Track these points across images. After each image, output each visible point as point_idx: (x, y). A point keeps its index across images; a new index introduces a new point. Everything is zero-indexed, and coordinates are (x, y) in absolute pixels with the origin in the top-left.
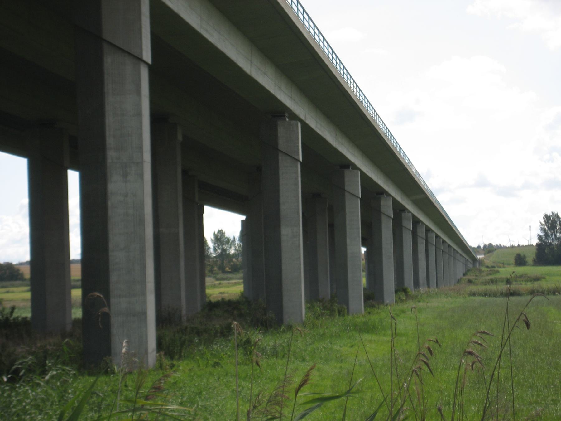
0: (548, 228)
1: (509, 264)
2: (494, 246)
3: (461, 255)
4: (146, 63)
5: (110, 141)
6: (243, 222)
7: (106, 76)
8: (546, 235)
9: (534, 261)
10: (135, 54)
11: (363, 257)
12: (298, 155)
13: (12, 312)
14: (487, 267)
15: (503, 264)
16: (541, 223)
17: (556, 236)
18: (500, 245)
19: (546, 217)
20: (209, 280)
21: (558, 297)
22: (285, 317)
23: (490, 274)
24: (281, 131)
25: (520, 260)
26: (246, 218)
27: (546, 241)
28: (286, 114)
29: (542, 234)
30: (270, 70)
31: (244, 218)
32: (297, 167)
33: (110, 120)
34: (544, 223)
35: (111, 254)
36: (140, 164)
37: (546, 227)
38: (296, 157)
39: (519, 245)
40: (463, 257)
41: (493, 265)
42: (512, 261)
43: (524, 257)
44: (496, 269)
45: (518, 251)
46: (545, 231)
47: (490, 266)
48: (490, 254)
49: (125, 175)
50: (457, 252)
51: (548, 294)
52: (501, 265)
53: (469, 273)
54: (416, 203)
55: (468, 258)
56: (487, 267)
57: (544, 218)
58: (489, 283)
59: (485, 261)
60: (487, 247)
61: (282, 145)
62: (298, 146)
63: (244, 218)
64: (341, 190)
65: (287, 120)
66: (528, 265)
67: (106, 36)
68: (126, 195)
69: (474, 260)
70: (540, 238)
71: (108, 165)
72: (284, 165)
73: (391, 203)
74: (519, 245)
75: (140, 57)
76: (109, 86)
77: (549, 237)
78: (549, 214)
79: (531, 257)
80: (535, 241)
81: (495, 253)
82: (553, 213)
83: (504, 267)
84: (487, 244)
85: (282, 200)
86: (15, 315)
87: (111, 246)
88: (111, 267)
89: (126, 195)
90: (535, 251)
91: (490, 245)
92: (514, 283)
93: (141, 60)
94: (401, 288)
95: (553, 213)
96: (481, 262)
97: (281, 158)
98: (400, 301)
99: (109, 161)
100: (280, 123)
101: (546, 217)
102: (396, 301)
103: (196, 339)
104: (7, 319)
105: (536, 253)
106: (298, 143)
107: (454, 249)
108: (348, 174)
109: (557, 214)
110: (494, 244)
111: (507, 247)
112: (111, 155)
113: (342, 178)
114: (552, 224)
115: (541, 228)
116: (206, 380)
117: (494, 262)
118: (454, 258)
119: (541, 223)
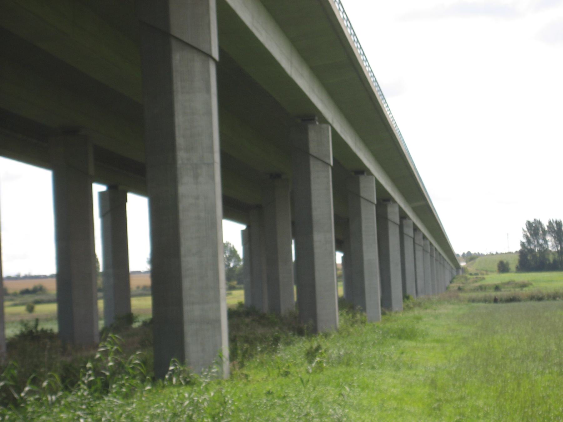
0: (531, 234)
1: (492, 272)
2: (473, 254)
3: (448, 263)
4: (214, 59)
5: (180, 141)
6: (243, 232)
7: (175, 74)
8: (529, 241)
9: (517, 268)
10: (205, 50)
11: (340, 267)
12: (329, 159)
13: (37, 325)
14: (471, 274)
15: (487, 271)
16: (523, 230)
17: (538, 242)
18: (478, 253)
19: (529, 224)
20: (7, 303)
21: (559, 302)
22: (320, 324)
23: (476, 281)
24: (312, 135)
25: (503, 267)
26: (247, 228)
27: (529, 247)
28: (317, 118)
29: (524, 240)
30: (306, 72)
31: (244, 227)
32: (328, 171)
33: (180, 119)
34: (526, 230)
35: (183, 259)
36: (211, 165)
37: (528, 234)
38: (327, 161)
39: (497, 253)
40: (450, 265)
41: (476, 272)
42: (496, 268)
43: (507, 264)
44: (480, 276)
45: (498, 259)
46: (527, 237)
47: (473, 273)
48: (472, 261)
49: (196, 177)
50: (445, 260)
51: (548, 299)
52: (484, 272)
53: (455, 280)
54: (415, 210)
55: (453, 266)
56: (471, 274)
57: (526, 225)
58: (477, 290)
59: (469, 268)
60: (465, 255)
61: (313, 149)
62: (329, 150)
63: (244, 227)
64: (357, 196)
65: (317, 123)
66: (512, 272)
67: (175, 31)
68: (197, 198)
69: (458, 267)
70: (523, 244)
71: (178, 166)
72: (315, 168)
73: (397, 210)
74: (497, 253)
75: (209, 53)
76: (178, 84)
77: (532, 244)
78: (532, 220)
79: (513, 264)
80: (519, 248)
81: (477, 260)
82: (535, 220)
83: (487, 274)
84: (466, 252)
85: (314, 205)
86: (39, 328)
87: (183, 250)
88: (184, 273)
89: (197, 198)
90: (517, 257)
91: (469, 253)
92: (503, 290)
93: (210, 56)
94: (406, 297)
95: (535, 220)
96: (464, 270)
97: (312, 162)
98: (408, 308)
99: (179, 162)
100: (310, 127)
101: (529, 224)
102: (404, 309)
103: (258, 348)
104: (31, 332)
105: (519, 260)
106: (329, 147)
107: (443, 258)
108: (363, 179)
109: (539, 221)
110: (472, 252)
111: (504, 254)
112: (181, 155)
113: (357, 184)
114: (534, 230)
115: (524, 235)
116: (223, 393)
117: (477, 270)
118: (444, 266)
119: (523, 230)
